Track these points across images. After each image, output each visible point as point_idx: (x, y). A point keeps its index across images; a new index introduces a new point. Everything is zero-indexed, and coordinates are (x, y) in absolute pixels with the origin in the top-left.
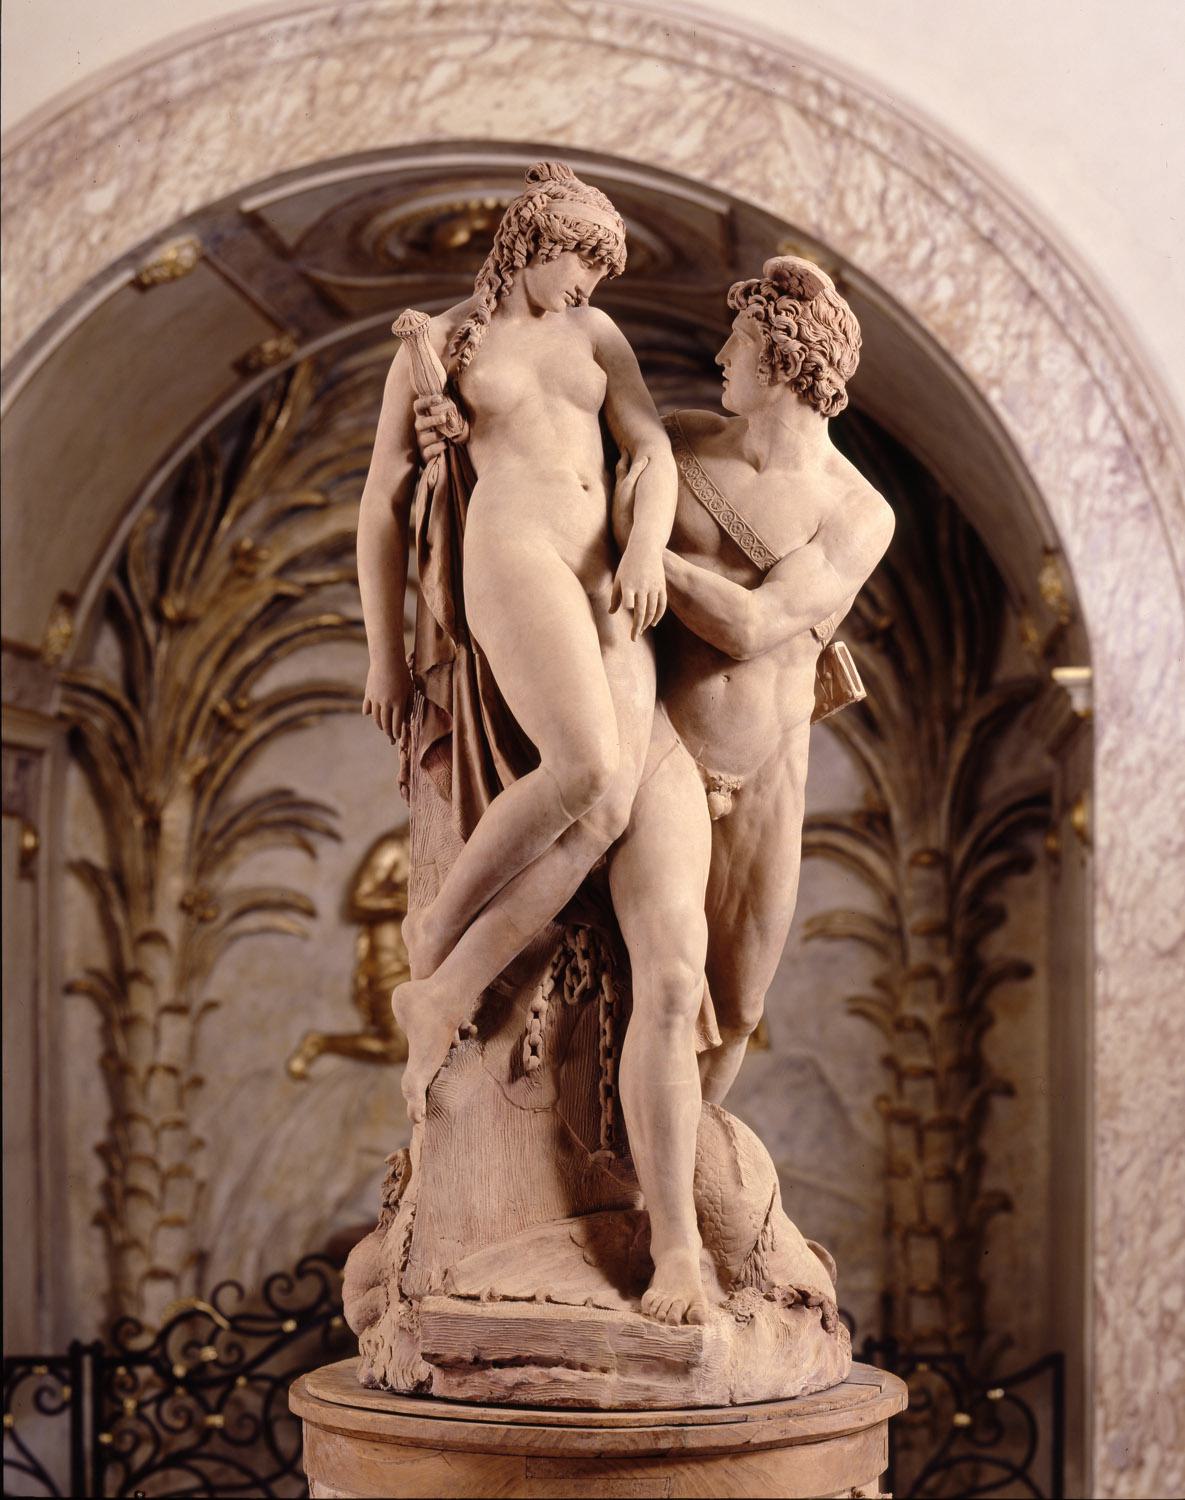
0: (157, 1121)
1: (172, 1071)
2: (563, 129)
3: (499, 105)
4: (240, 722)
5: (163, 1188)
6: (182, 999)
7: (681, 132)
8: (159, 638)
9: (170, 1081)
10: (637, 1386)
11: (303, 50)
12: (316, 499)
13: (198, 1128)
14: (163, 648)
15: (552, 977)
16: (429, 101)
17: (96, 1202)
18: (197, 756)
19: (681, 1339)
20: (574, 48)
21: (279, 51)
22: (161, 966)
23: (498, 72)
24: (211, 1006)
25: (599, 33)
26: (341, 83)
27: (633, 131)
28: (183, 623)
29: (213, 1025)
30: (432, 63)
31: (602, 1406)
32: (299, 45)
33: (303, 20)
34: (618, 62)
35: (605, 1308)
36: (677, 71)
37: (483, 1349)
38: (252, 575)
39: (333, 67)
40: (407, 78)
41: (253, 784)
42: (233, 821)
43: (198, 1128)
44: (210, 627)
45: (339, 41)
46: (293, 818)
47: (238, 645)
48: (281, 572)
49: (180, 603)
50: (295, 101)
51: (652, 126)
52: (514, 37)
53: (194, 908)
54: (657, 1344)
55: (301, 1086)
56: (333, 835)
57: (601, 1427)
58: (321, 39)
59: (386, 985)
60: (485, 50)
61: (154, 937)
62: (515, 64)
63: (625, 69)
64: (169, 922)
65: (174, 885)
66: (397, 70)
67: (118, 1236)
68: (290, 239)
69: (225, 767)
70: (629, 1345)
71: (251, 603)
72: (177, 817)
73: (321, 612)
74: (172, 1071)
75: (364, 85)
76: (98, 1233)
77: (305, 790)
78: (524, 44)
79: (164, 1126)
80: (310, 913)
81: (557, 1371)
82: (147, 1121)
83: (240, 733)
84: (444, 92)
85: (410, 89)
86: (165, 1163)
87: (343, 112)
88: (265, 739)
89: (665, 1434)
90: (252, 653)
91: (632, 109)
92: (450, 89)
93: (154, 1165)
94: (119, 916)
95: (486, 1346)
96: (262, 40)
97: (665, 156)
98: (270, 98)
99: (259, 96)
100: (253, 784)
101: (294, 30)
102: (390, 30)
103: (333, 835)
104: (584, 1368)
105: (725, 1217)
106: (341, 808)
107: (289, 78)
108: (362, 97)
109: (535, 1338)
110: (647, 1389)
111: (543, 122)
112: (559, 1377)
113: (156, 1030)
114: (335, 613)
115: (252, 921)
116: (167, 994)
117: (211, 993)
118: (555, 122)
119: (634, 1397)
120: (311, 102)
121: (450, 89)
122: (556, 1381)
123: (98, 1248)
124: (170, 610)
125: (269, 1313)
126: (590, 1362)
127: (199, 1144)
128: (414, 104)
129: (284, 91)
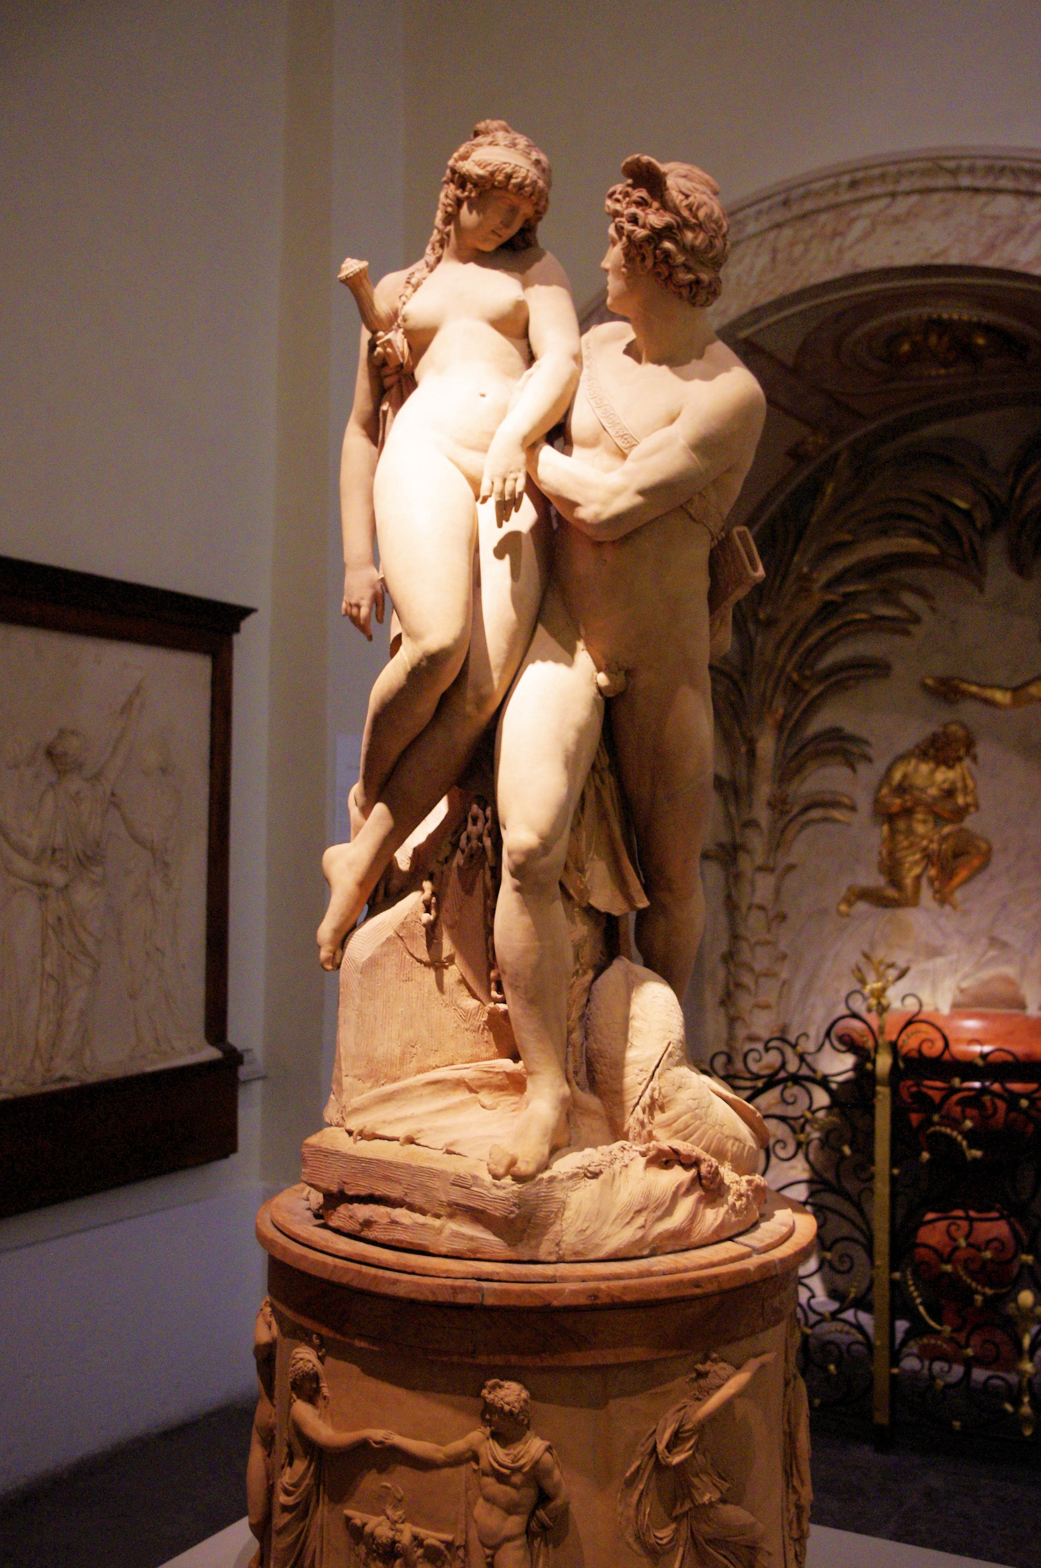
0: (753, 940)
1: (761, 908)
2: (943, 252)
3: (897, 243)
4: (806, 686)
5: (756, 982)
6: (771, 862)
7: (1026, 243)
8: (756, 633)
9: (761, 915)
10: (463, 1235)
11: (766, 225)
12: (848, 537)
13: (783, 946)
14: (759, 640)
15: (450, 843)
16: (851, 247)
17: (720, 990)
18: (779, 706)
19: (501, 1193)
20: (950, 195)
21: (751, 228)
22: (757, 842)
23: (897, 220)
24: (791, 867)
25: (965, 181)
26: (792, 245)
27: (991, 247)
28: (770, 623)
29: (792, 882)
30: (853, 221)
31: (431, 1251)
32: (765, 222)
33: (767, 204)
34: (981, 199)
35: (459, 1154)
36: (1024, 200)
37: (345, 1183)
38: (808, 590)
39: (787, 233)
40: (836, 234)
41: (818, 724)
42: (802, 748)
43: (783, 946)
44: (784, 627)
45: (789, 216)
46: (842, 747)
47: (804, 633)
48: (829, 586)
49: (769, 610)
50: (764, 259)
51: (1005, 241)
52: (908, 193)
53: (778, 804)
54: (481, 1197)
55: (845, 921)
56: (869, 760)
57: (413, 1273)
58: (778, 216)
59: (899, 855)
60: (888, 206)
61: (752, 824)
62: (909, 213)
63: (985, 205)
64: (763, 815)
65: (764, 790)
66: (829, 229)
67: (732, 1012)
68: (790, 362)
69: (796, 715)
70: (457, 1195)
71: (807, 608)
72: (766, 745)
73: (857, 611)
74: (761, 908)
75: (807, 243)
76: (722, 1011)
77: (849, 728)
78: (914, 199)
79: (758, 943)
80: (853, 808)
81: (401, 1214)
82: (747, 939)
83: (806, 693)
84: (858, 241)
85: (838, 241)
86: (757, 968)
87: (794, 263)
88: (821, 696)
89: (463, 1289)
90: (812, 640)
91: (990, 232)
92: (866, 236)
93: (752, 970)
94: (732, 809)
95: (348, 1181)
96: (740, 222)
97: (1013, 262)
98: (747, 260)
99: (740, 261)
100: (818, 724)
101: (760, 212)
102: (822, 203)
103: (869, 760)
104: (423, 1212)
105: (612, 1072)
106: (872, 740)
107: (759, 246)
108: (806, 250)
109: (386, 1178)
110: (472, 1239)
111: (928, 249)
112: (397, 1219)
113: (752, 883)
114: (864, 611)
115: (815, 814)
116: (759, 861)
117: (791, 860)
118: (936, 249)
119: (459, 1246)
120: (774, 259)
121: (866, 236)
122: (394, 1222)
123: (722, 1019)
124: (762, 616)
125: (748, 1075)
126: (426, 1207)
127: (784, 957)
128: (840, 251)
129: (756, 255)
